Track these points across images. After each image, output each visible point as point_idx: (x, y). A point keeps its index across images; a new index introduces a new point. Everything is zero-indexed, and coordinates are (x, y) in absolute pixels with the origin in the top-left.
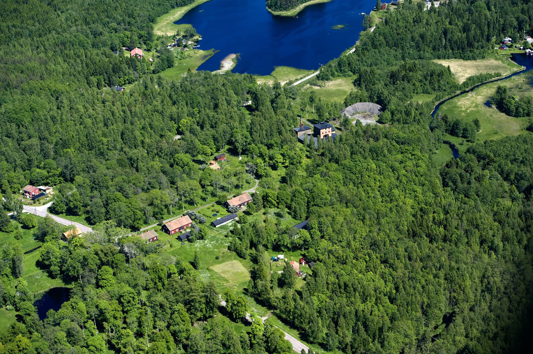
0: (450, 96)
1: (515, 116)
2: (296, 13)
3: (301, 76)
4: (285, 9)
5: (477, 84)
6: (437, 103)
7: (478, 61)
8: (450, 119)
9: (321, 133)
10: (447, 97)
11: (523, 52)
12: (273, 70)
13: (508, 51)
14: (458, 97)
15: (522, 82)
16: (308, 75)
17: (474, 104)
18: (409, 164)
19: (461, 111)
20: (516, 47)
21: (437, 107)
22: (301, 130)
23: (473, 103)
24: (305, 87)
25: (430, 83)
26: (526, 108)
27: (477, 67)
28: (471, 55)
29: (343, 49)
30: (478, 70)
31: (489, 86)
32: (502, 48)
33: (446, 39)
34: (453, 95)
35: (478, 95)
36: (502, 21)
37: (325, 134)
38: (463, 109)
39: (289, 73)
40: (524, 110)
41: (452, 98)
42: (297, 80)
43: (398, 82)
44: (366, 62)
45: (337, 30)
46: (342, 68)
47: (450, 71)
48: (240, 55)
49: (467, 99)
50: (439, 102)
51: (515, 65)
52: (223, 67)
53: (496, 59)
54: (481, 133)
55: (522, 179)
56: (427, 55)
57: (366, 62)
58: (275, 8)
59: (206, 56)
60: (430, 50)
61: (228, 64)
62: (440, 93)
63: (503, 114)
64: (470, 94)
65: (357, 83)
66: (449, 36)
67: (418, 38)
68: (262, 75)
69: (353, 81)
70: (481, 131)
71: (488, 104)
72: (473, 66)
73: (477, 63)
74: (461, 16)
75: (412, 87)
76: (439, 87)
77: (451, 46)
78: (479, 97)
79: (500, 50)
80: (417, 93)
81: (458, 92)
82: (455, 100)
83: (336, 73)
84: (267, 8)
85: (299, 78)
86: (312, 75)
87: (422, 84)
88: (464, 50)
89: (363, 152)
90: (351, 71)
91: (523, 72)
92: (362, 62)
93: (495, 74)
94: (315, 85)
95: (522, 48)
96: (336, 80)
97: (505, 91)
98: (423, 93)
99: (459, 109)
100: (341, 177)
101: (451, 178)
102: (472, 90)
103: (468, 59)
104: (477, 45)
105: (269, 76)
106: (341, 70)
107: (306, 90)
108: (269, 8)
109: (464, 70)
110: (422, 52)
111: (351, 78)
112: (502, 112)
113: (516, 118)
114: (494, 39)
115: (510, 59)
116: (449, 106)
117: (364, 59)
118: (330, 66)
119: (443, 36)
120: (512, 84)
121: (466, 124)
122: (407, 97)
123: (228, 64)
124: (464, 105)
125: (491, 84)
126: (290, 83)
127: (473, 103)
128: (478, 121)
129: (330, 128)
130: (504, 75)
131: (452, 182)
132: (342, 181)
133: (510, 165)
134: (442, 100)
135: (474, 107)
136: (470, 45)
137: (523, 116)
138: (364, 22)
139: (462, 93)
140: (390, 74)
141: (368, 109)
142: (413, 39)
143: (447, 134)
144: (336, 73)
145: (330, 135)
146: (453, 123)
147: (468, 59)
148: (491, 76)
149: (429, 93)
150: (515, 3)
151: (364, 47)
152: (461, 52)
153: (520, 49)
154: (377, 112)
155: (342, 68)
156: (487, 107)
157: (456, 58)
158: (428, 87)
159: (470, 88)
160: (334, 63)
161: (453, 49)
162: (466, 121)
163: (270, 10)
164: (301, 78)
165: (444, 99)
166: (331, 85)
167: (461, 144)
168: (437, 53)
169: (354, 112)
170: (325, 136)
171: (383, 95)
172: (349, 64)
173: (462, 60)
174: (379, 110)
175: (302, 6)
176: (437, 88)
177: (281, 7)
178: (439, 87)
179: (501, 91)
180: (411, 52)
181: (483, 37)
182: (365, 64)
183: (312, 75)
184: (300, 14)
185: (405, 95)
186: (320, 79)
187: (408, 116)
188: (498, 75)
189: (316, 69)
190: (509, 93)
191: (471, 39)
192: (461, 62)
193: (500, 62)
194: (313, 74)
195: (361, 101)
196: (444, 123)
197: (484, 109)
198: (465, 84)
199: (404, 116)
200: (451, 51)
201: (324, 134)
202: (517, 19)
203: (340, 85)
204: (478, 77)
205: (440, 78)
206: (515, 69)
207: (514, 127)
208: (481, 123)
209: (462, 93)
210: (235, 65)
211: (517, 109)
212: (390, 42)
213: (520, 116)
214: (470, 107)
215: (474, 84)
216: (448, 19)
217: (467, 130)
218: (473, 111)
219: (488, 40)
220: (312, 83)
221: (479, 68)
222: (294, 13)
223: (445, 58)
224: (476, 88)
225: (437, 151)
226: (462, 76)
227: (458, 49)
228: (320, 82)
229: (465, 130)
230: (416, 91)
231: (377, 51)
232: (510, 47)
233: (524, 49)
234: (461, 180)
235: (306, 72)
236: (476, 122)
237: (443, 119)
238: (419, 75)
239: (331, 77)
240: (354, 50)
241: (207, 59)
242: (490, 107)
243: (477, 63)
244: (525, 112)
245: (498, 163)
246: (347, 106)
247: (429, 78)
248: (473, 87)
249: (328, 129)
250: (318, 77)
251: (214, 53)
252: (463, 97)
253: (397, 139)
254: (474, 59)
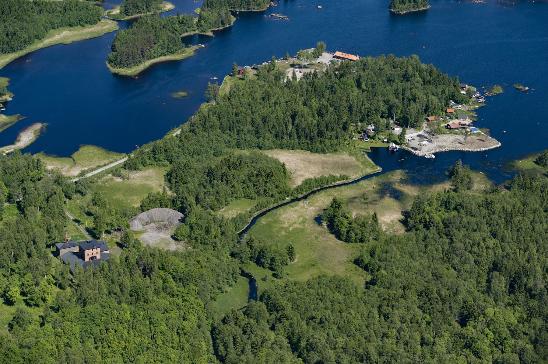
0: (276, 205)
1: (346, 241)
2: (138, 71)
3: (106, 161)
4: (126, 66)
5: (315, 189)
6: (256, 214)
7: (328, 155)
8: (256, 245)
9: (86, 255)
10: (271, 206)
11: (386, 145)
12: (77, 149)
13: (368, 144)
14: (285, 206)
15: (371, 189)
16: (116, 160)
17: (301, 219)
18: (174, 314)
19: (282, 228)
20: (379, 139)
21: (255, 219)
22: (64, 247)
23: (300, 216)
24: (105, 178)
25: (254, 185)
26: (359, 232)
27: (323, 164)
28: (320, 146)
29: (171, 128)
30: (323, 168)
31: (329, 193)
32: (361, 139)
33: (293, 124)
34: (280, 203)
35: (311, 206)
36: (368, 105)
37: (91, 256)
38: (285, 226)
39: (95, 155)
40: (356, 235)
41: (277, 207)
42: (92, 170)
43: (215, 181)
44: (188, 149)
45: (176, 99)
46: (157, 156)
47: (284, 169)
48: (47, 126)
49: (296, 211)
50: (259, 212)
51: (370, 164)
52: (19, 141)
53: (350, 154)
54: (295, 264)
55: (313, 349)
56: (267, 143)
57: (188, 149)
58: (115, 64)
59: (5, 124)
60: (272, 137)
61: (27, 138)
62: (263, 200)
63: (333, 236)
64: (301, 203)
65: (169, 177)
66: (297, 121)
67: (259, 121)
68: (61, 157)
69: (165, 173)
70: (296, 260)
71: (318, 220)
72: (318, 163)
73: (325, 159)
74: (320, 96)
75: (229, 189)
76: (265, 191)
77: (297, 133)
78: (311, 208)
79: (359, 142)
80: (236, 198)
81: (288, 199)
82: (281, 210)
83: (148, 161)
84: (107, 62)
85: (103, 164)
86: (119, 162)
87: (245, 186)
88: (311, 139)
89: (119, 293)
90: (167, 160)
91: (377, 174)
92: (183, 149)
93: (341, 176)
94: (119, 176)
95: (385, 140)
96: (146, 170)
97: (339, 206)
98: (245, 197)
99: (281, 225)
100: (77, 330)
101: (223, 340)
102: (305, 197)
103: (317, 151)
104: (329, 134)
105: (67, 159)
106: (155, 158)
107: (104, 182)
108: (109, 63)
109: (306, 168)
110: (261, 139)
111: (165, 169)
112: (332, 233)
113: (346, 244)
114: (352, 128)
115: (366, 156)
116: (270, 219)
117: (186, 145)
118: (142, 152)
119: (290, 120)
120: (358, 191)
121: (275, 252)
122: (221, 203)
123: (27, 138)
124: (289, 220)
125: (332, 190)
126: (83, 173)
127: (300, 216)
128: (292, 248)
129: (99, 249)
130: (353, 177)
131: (224, 345)
132: (78, 336)
133: (304, 326)
134: (264, 210)
135: (300, 223)
136: (321, 134)
137: (356, 242)
138: (207, 92)
139: (293, 201)
140: (207, 171)
141: (166, 218)
142: (253, 122)
143: (250, 262)
144: (148, 161)
145: (98, 257)
146: (259, 250)
147: (317, 152)
148: (334, 179)
149: (252, 199)
150: (391, 80)
151: (192, 128)
152: (309, 142)
153: (383, 142)
154: (176, 222)
155: (157, 156)
156: (316, 225)
157: (302, 149)
158: (252, 190)
159: (305, 194)
160: (147, 148)
161: (299, 138)
162: (275, 248)
163: (109, 65)
164: (105, 165)
165: (267, 209)
166: (137, 178)
167: (264, 280)
168: (279, 142)
169: (149, 220)
170: (92, 258)
171: (187, 201)
172: (166, 151)
173: (308, 153)
174: (179, 220)
175: (148, 63)
176: (262, 192)
177: (121, 63)
178: (265, 191)
179: (336, 204)
180: (248, 139)
181: (338, 124)
182: (187, 151)
183: (119, 162)
184: (143, 74)
185: (218, 201)
186: (127, 167)
187: (207, 234)
188: (344, 178)
189: (128, 152)
190: (344, 208)
191: (323, 127)
192: (308, 155)
193: (354, 159)
194: (123, 159)
195: (161, 206)
196: (248, 249)
197: (311, 227)
198: (299, 189)
199: (204, 234)
200: (297, 140)
201: (90, 256)
202: (387, 102)
203: (148, 178)
204: (316, 180)
205: (268, 180)
206: (369, 171)
207: (338, 257)
208: (296, 250)
209: (293, 201)
210: (34, 139)
211: (348, 232)
212: (224, 125)
213: (352, 242)
214: (295, 223)
215: (312, 189)
216: (303, 98)
217: (274, 261)
218: (296, 229)
219: (345, 128)
220: (116, 172)
221: (326, 166)
222: (135, 71)
223: (289, 149)
224: (311, 195)
225: (229, 289)
226: (302, 176)
227: (306, 138)
228: (123, 172)
229: (273, 260)
230: (235, 195)
231: (206, 134)
232: (373, 138)
233: (388, 142)
234: (234, 344)
235: (117, 157)
236: (290, 252)
237: (247, 243)
238: (242, 175)
239: (141, 167)
240: (179, 132)
241: (5, 128)
242: (320, 224)
243: (325, 159)
244: (358, 237)
245: (290, 321)
246: (143, 211)
247: (254, 179)
248: (309, 192)
249: (95, 250)
250: (125, 166)
251: (17, 121)
252: (292, 206)
253: (174, 274)
254: (324, 152)
